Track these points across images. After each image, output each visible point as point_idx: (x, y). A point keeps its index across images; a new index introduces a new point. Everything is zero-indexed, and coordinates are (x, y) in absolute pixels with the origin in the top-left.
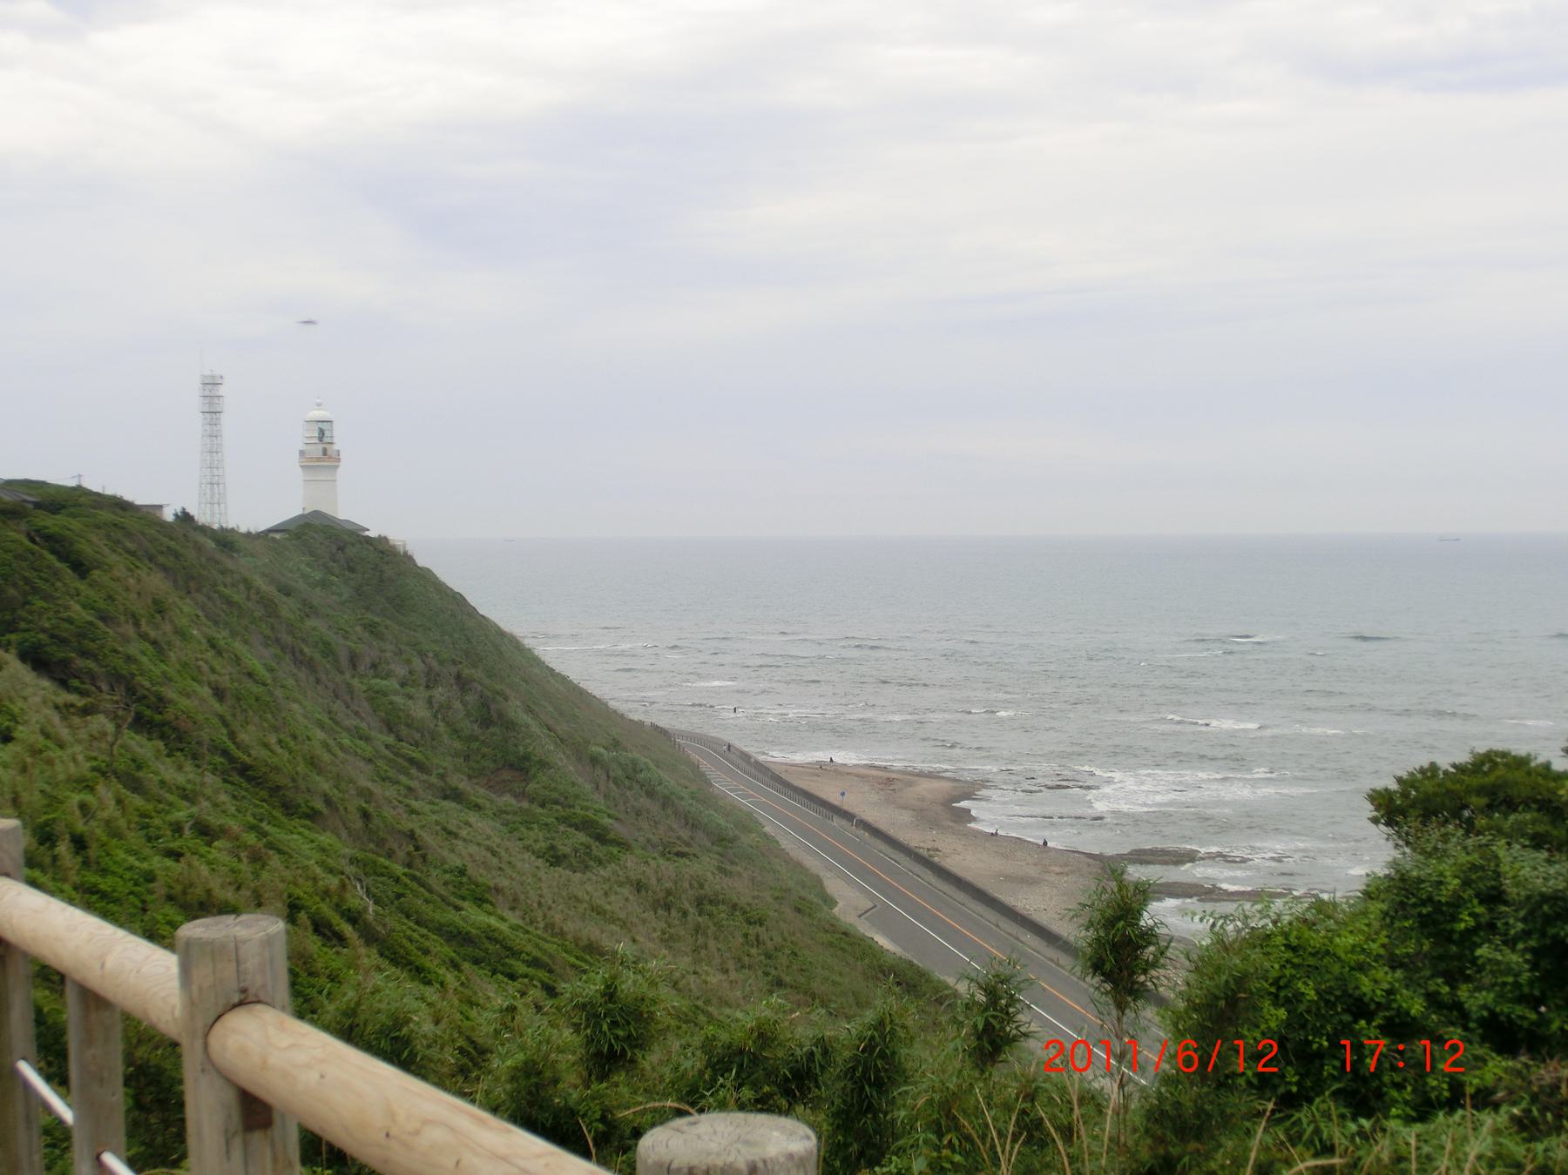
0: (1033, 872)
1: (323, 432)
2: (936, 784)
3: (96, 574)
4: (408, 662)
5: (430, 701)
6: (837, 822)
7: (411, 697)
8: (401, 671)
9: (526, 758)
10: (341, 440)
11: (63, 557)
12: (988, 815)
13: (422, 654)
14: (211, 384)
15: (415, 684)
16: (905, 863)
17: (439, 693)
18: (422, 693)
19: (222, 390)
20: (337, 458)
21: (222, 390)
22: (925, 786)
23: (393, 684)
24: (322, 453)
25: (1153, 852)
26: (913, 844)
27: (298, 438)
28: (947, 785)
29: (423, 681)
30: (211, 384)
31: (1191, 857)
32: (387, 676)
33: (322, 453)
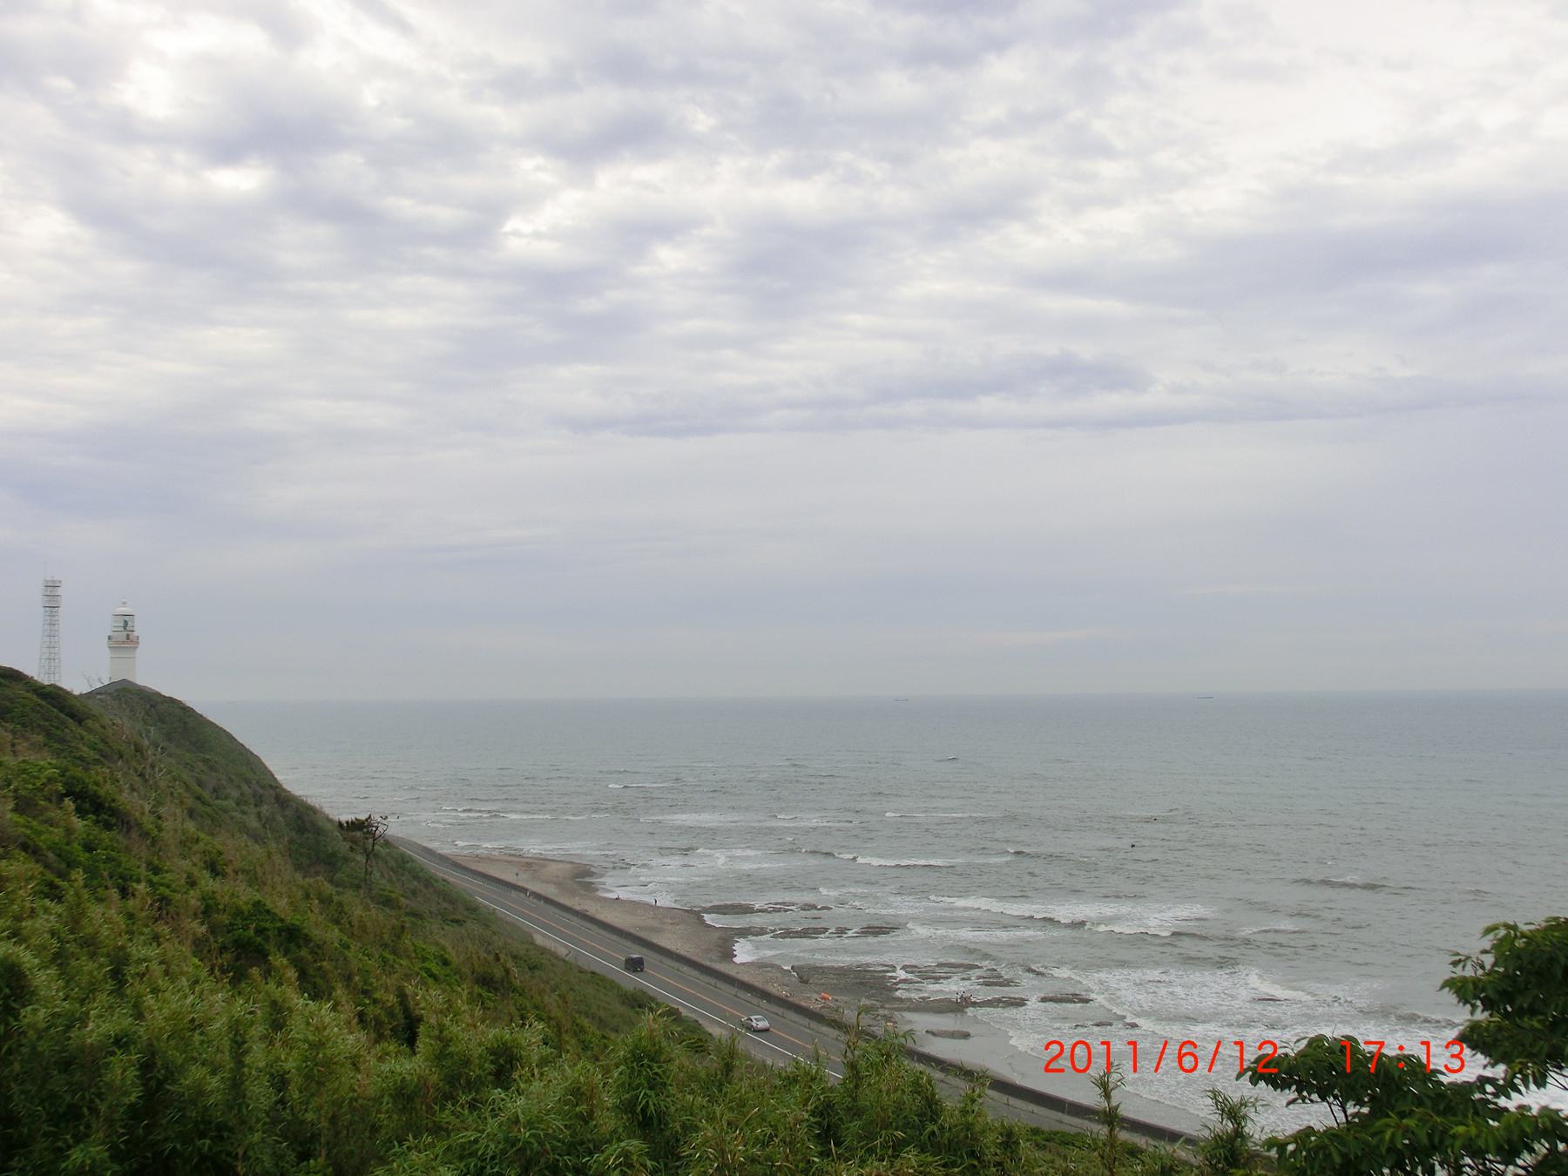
0: (655, 924)
1: (126, 622)
2: (561, 866)
3: (89, 722)
4: (239, 787)
5: (259, 815)
6: (514, 894)
7: (244, 813)
8: (235, 794)
9: (334, 855)
10: (139, 631)
11: (61, 710)
12: (615, 887)
13: (247, 782)
14: (52, 587)
15: (246, 804)
16: (576, 922)
17: (265, 809)
18: (252, 810)
19: (60, 591)
20: (136, 641)
21: (60, 591)
22: (554, 866)
23: (231, 803)
24: (125, 638)
25: (726, 907)
26: (578, 908)
27: (108, 627)
28: (568, 866)
29: (252, 801)
30: (52, 587)
31: (747, 910)
32: (226, 798)
33: (125, 638)
